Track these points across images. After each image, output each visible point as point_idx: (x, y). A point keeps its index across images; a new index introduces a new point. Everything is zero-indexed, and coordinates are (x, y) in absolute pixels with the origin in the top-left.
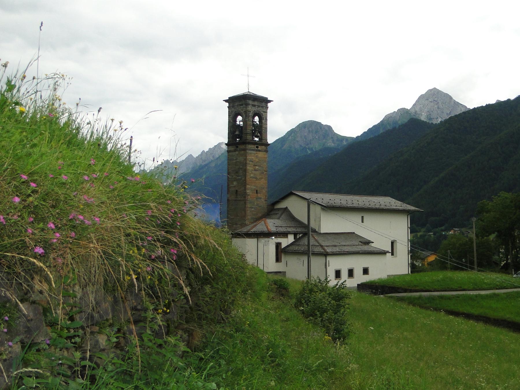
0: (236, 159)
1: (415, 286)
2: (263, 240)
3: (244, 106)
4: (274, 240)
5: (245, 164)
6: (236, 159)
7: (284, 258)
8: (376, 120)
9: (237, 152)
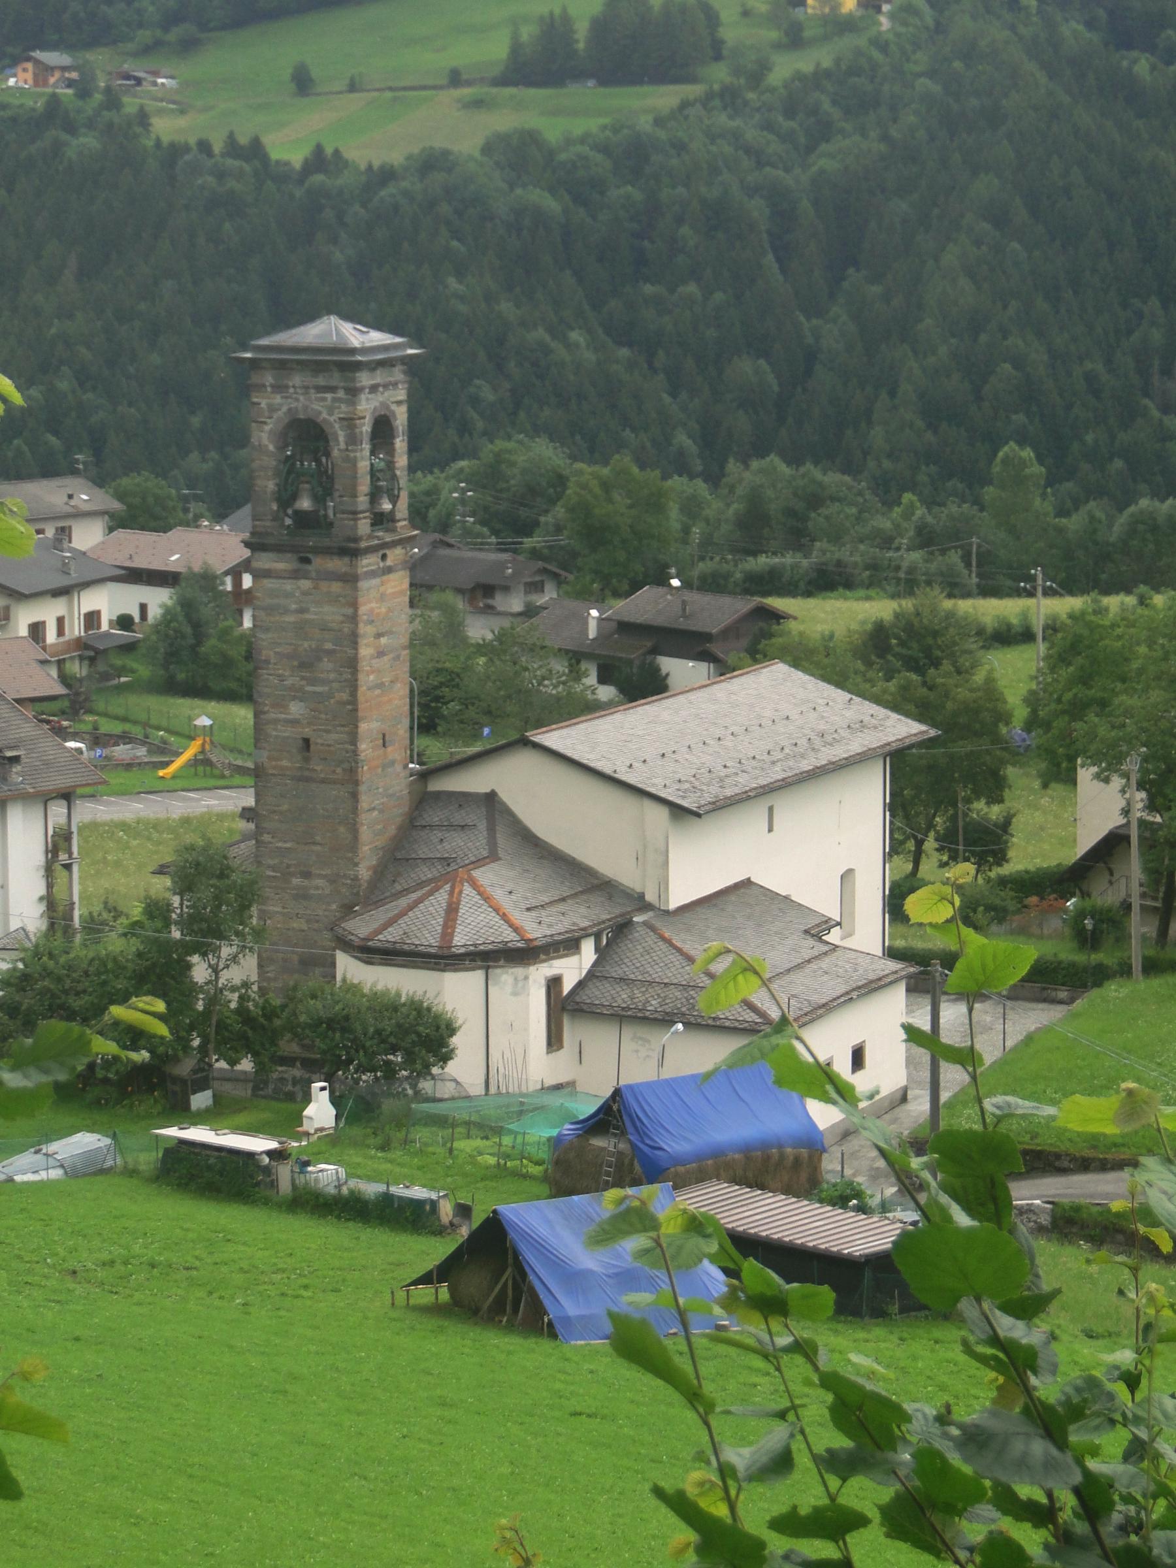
0: (302, 611)
1: (1115, 1145)
2: (506, 977)
3: (341, 394)
4: (540, 973)
5: (354, 639)
6: (302, 611)
7: (570, 1031)
8: (1106, 832)
9: (305, 584)
